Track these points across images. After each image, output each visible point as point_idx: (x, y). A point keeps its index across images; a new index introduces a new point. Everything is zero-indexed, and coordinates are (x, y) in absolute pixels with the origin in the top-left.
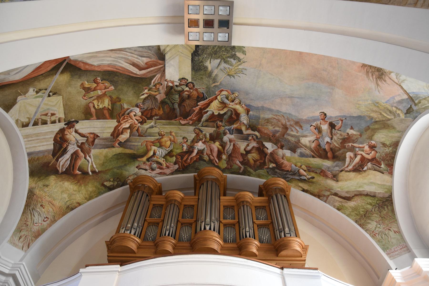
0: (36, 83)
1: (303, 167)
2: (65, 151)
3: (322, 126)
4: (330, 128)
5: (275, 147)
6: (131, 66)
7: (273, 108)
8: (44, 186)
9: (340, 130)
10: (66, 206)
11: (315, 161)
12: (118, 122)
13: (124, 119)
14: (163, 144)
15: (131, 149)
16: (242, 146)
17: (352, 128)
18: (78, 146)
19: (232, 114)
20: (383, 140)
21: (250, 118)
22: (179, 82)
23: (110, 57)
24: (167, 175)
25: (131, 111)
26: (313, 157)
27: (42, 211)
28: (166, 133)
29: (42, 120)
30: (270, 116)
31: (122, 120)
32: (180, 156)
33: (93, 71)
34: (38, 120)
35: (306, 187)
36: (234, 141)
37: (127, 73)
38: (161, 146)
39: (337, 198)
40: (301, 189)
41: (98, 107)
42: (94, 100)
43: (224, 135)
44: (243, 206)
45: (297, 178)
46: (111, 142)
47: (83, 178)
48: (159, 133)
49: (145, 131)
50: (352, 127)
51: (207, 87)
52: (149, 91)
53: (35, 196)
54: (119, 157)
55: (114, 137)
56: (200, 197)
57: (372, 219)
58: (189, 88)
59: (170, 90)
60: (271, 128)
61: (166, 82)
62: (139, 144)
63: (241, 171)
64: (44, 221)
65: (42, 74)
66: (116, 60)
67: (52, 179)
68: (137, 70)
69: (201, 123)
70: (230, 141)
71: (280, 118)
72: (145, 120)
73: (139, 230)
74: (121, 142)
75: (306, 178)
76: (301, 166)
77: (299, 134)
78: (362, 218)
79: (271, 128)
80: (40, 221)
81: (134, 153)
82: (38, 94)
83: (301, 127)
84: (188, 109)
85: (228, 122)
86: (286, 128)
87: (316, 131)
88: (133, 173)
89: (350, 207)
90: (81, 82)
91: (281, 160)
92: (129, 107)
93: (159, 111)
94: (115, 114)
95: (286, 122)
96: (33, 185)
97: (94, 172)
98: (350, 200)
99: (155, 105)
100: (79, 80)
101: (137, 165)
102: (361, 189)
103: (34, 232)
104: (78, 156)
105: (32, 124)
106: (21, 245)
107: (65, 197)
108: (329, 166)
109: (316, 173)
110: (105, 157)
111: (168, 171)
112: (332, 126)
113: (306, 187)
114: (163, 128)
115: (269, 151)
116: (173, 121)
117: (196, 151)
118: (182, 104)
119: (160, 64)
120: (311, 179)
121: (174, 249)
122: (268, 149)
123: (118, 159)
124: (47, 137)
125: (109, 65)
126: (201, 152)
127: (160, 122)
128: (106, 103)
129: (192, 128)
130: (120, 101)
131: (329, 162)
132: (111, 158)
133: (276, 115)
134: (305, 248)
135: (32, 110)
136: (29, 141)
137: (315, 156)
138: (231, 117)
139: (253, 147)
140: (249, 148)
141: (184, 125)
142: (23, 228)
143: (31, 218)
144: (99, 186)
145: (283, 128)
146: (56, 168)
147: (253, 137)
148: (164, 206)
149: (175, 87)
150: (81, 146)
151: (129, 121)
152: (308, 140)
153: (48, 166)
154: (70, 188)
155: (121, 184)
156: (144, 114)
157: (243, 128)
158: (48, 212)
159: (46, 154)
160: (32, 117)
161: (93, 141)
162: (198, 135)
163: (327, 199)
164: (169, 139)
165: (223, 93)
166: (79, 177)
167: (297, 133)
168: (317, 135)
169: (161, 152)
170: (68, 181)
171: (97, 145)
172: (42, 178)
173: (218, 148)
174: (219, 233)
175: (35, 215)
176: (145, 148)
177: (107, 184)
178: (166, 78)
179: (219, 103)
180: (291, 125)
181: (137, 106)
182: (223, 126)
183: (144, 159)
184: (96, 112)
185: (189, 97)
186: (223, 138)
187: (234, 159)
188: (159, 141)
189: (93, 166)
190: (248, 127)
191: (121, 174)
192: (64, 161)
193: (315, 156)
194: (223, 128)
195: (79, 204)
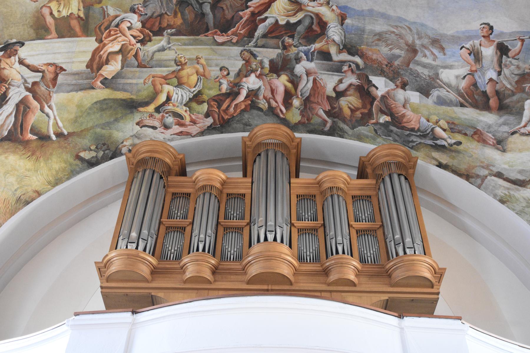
1: (442, 123)
3: (483, 49)
4: (499, 53)
5: (392, 86)
7: (391, 13)
10: (15, 198)
11: (464, 114)
12: (100, 41)
13: (109, 35)
14: (185, 80)
15: (125, 91)
16: (330, 82)
18: (27, 89)
19: (312, 23)
25: (122, 21)
26: (462, 105)
28: (189, 59)
31: (105, 38)
35: (444, 159)
38: (180, 84)
39: (501, 182)
40: (437, 163)
41: (59, 15)
43: (297, 63)
44: (332, 196)
45: (430, 142)
46: (87, 78)
47: (42, 146)
48: (175, 60)
54: (105, 107)
55: (92, 69)
56: (255, 180)
60: (384, 50)
62: (139, 82)
63: (327, 128)
69: (254, 40)
70: (308, 73)
71: (403, 32)
72: (149, 36)
73: (152, 241)
74: (106, 79)
77: (438, 63)
81: (131, 99)
83: (442, 49)
84: (229, 14)
85: (304, 38)
86: (413, 50)
87: (471, 59)
88: (132, 134)
89: (525, 199)
91: (402, 109)
92: (118, 13)
94: (92, 26)
97: (59, 135)
98: (524, 186)
99: (168, 7)
101: (137, 120)
104: (29, 108)
108: (491, 123)
109: (466, 134)
110: (79, 106)
111: (194, 129)
112: (503, 49)
113: (444, 159)
114: (183, 50)
115: (379, 93)
116: (202, 37)
117: (244, 93)
118: (219, 5)
120: (455, 146)
121: (214, 273)
122: (377, 88)
123: (102, 110)
126: (253, 94)
129: (237, 50)
132: (90, 108)
133: (397, 27)
134: (439, 274)
137: (466, 104)
138: (310, 28)
139: (351, 85)
140: (342, 87)
141: (222, 44)
144: (71, 160)
145: (408, 50)
147: (350, 66)
148: (192, 196)
150: (32, 89)
151: (120, 39)
156: (147, 25)
157: (333, 50)
161: (55, 79)
162: (248, 62)
163: (483, 181)
164: (194, 71)
166: (34, 145)
168: (472, 66)
169: (181, 96)
170: (14, 152)
171: (61, 85)
173: (285, 87)
174: (290, 246)
176: (151, 89)
180: (423, 46)
181: (133, 10)
182: (295, 46)
183: (151, 108)
184: (56, 25)
186: (294, 68)
187: (314, 105)
188: (176, 74)
189: (57, 123)
190: (341, 47)
191: (110, 136)
193: (466, 104)
194: (293, 51)
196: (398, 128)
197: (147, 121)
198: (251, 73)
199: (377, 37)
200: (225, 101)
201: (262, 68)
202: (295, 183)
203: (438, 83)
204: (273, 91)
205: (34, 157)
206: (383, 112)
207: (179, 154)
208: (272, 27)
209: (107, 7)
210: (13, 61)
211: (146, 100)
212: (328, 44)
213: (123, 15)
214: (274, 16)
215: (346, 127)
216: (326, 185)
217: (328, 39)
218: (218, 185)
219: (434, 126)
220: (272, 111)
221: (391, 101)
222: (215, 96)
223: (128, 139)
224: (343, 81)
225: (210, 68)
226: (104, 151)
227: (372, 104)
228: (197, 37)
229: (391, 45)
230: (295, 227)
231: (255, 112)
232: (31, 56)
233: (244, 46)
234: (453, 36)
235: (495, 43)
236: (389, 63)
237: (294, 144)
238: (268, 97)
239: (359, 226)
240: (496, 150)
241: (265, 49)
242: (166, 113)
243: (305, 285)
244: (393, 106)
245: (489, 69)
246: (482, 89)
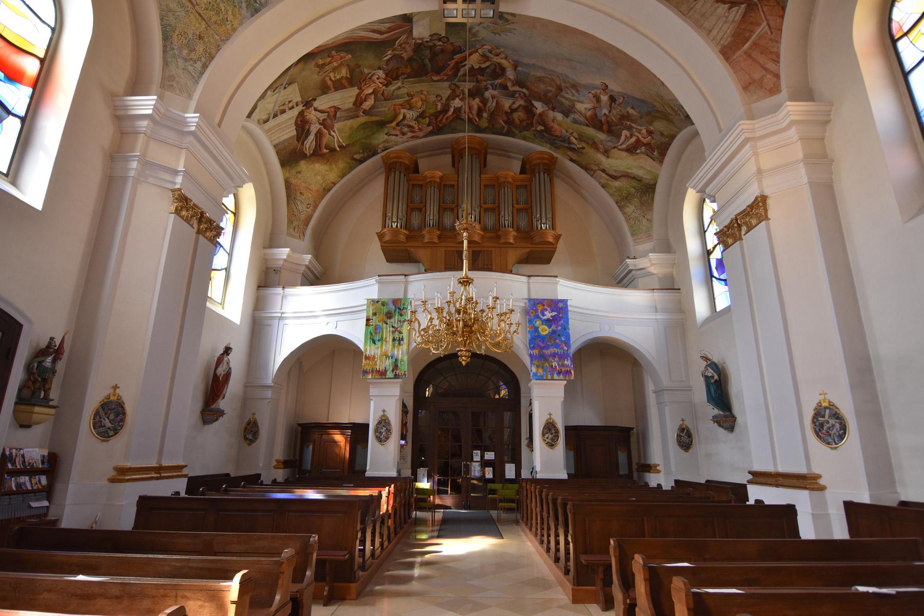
1: (575, 134)
2: (308, 133)
5: (546, 108)
7: (546, 67)
12: (360, 88)
16: (507, 103)
17: (633, 108)
18: (320, 124)
20: (661, 129)
25: (373, 75)
26: (587, 126)
30: (543, 75)
35: (574, 157)
38: (411, 108)
39: (604, 175)
45: (566, 145)
59: (419, 47)
60: (542, 87)
62: (386, 109)
67: (303, 165)
70: (493, 97)
77: (574, 98)
78: (623, 200)
86: (560, 89)
87: (594, 100)
96: (288, 175)
97: (341, 147)
101: (386, 131)
102: (629, 171)
106: (297, 235)
110: (351, 128)
111: (421, 134)
112: (612, 99)
115: (538, 112)
116: (424, 78)
117: (452, 110)
126: (458, 110)
128: (344, 72)
129: (447, 84)
134: (557, 238)
138: (494, 71)
140: (515, 106)
150: (323, 123)
152: (584, 106)
157: (509, 84)
161: (335, 115)
162: (454, 91)
169: (411, 114)
177: (357, 157)
181: (380, 68)
183: (394, 124)
185: (442, 51)
188: (409, 102)
194: (484, 83)
195: (335, 184)
204: (470, 108)
206: (540, 124)
215: (516, 131)
216: (501, 180)
218: (438, 180)
220: (470, 120)
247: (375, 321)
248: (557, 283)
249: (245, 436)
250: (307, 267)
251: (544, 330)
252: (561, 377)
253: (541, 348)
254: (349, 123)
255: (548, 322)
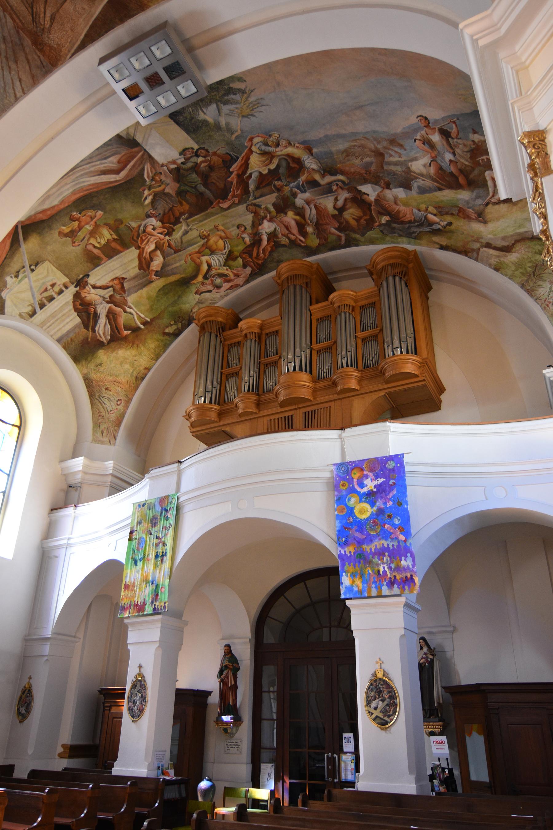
0: (7, 270)
1: (431, 209)
2: (96, 317)
3: (431, 137)
4: (445, 138)
5: (379, 189)
6: (103, 176)
7: (343, 132)
8: (97, 366)
9: (459, 137)
11: (444, 196)
12: (138, 247)
13: (142, 241)
14: (214, 247)
15: (175, 274)
16: (328, 204)
18: (108, 302)
21: (318, 158)
22: (183, 156)
23: (66, 184)
24: (242, 286)
25: (145, 227)
26: (440, 189)
27: (110, 395)
28: (210, 230)
29: (46, 298)
31: (141, 244)
32: (246, 253)
33: (60, 211)
34: (41, 300)
35: (444, 241)
36: (313, 200)
37: (104, 187)
38: (212, 252)
39: (491, 252)
41: (100, 245)
42: (88, 240)
45: (427, 229)
46: (144, 277)
47: (137, 336)
48: (200, 236)
49: (180, 242)
50: (473, 130)
51: (227, 144)
52: (149, 190)
53: (94, 382)
55: (144, 270)
57: (544, 278)
58: (202, 157)
59: (178, 173)
60: (357, 162)
61: (165, 168)
62: (181, 263)
64: (118, 405)
65: (5, 258)
66: (77, 182)
67: (102, 355)
68: (114, 176)
69: (252, 194)
70: (308, 202)
71: (363, 142)
72: (171, 227)
74: (157, 271)
75: (439, 227)
76: (427, 209)
79: (357, 162)
80: (114, 407)
81: (182, 277)
82: (20, 277)
84: (221, 185)
86: (380, 155)
87: (426, 147)
88: (195, 302)
89: (512, 263)
90: (57, 232)
91: (395, 206)
92: (139, 223)
93: (183, 207)
95: (375, 146)
96: (85, 371)
97: (145, 323)
100: (52, 232)
101: (194, 290)
102: (522, 230)
103: (113, 421)
104: (116, 314)
105: (38, 309)
106: (106, 440)
107: (127, 368)
108: (467, 199)
110: (149, 298)
111: (240, 281)
112: (445, 134)
114: (202, 226)
115: (372, 198)
116: (210, 210)
117: (265, 238)
119: (138, 153)
122: (368, 195)
123: (166, 294)
124: (65, 312)
125: (73, 193)
126: (272, 236)
127: (194, 221)
128: (107, 235)
129: (242, 208)
130: (122, 223)
131: (464, 192)
132: (157, 296)
135: (27, 295)
136: (49, 327)
137: (443, 187)
138: (289, 168)
139: (346, 200)
140: (340, 203)
141: (229, 208)
142: (100, 421)
143: (103, 407)
144: (161, 337)
146: (99, 340)
149: (182, 166)
150: (111, 300)
151: (151, 240)
152: (420, 164)
153: (88, 343)
154: (128, 355)
155: (187, 323)
157: (317, 177)
158: (118, 393)
159: (77, 330)
160: (32, 302)
161: (123, 287)
162: (256, 213)
163: (478, 254)
164: (218, 237)
165: (256, 140)
166: (131, 337)
167: (400, 157)
168: (431, 154)
169: (216, 260)
170: (120, 348)
171: (129, 289)
172: (89, 359)
173: (295, 220)
175: (105, 403)
176: (193, 264)
177: (169, 330)
178: (161, 163)
179: (260, 156)
180: (385, 148)
181: (148, 216)
182: (286, 186)
183: (200, 278)
184: (102, 252)
185: (211, 168)
186: (294, 203)
187: (325, 227)
188: (206, 246)
189: (140, 316)
192: (103, 328)
193: (443, 187)
194: (287, 189)
195: (148, 369)
196: (399, 224)
197: (202, 289)
198: (263, 220)
199: (345, 154)
200: (253, 251)
201: (270, 212)
202: (314, 309)
203: (413, 175)
204: (287, 227)
205: (135, 346)
206: (382, 214)
207: (228, 310)
208: (259, 179)
209: (129, 224)
210: (88, 289)
211: (194, 274)
212: (310, 174)
213: (144, 223)
214: (256, 169)
215: (358, 236)
217: (308, 170)
219: (425, 214)
220: (293, 244)
221: (384, 203)
222: (243, 250)
223: (194, 306)
224: (339, 198)
225: (229, 230)
226: (181, 322)
227: (370, 210)
228: (207, 212)
229: (360, 156)
230: (314, 350)
231: (281, 249)
232: (99, 280)
233: (246, 202)
234: (403, 133)
235: (437, 129)
236: (367, 171)
237: (314, 269)
238: (286, 234)
239: (365, 335)
240: (479, 223)
241: (264, 198)
242: (213, 277)
243: (321, 398)
244: (387, 206)
245: (444, 152)
246: (449, 171)
247: (140, 534)
248: (386, 431)
249: (18, 709)
250: (112, 475)
251: (364, 511)
252: (396, 590)
253: (360, 543)
254: (144, 292)
255: (370, 497)
